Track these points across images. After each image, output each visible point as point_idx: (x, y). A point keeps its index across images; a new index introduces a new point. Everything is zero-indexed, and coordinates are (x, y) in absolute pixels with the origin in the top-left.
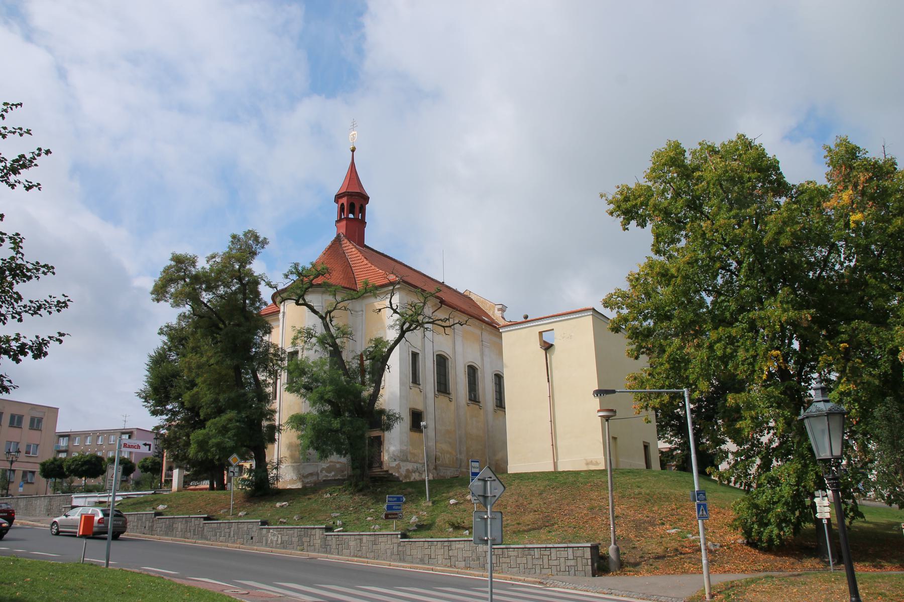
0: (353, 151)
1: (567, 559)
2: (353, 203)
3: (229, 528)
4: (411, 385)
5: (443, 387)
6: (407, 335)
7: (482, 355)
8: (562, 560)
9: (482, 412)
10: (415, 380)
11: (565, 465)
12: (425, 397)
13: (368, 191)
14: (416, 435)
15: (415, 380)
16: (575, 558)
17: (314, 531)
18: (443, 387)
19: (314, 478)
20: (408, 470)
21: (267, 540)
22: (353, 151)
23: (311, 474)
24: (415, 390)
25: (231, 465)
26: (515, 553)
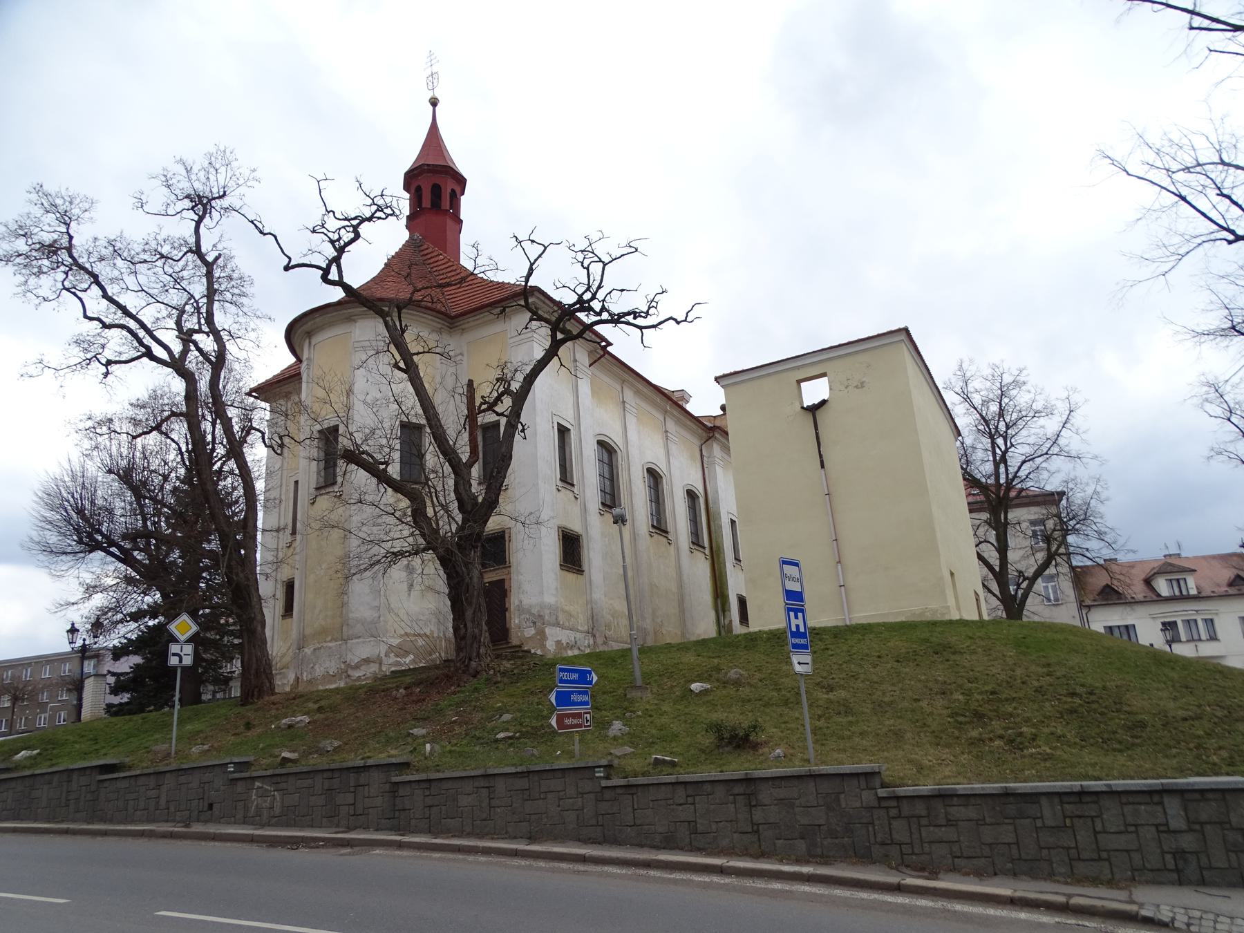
0: (434, 103)
1: (1163, 829)
2: (435, 187)
3: (158, 787)
4: (559, 483)
5: (611, 499)
6: (562, 351)
7: (668, 453)
8: (1148, 833)
9: (672, 548)
10: (566, 478)
11: (863, 614)
12: (585, 510)
13: (462, 167)
14: (571, 577)
15: (566, 478)
16: (1196, 826)
17: (363, 778)
18: (611, 499)
19: (374, 668)
20: (559, 643)
21: (246, 809)
22: (434, 103)
23: (367, 661)
24: (566, 495)
25: (176, 641)
26: (971, 812)
